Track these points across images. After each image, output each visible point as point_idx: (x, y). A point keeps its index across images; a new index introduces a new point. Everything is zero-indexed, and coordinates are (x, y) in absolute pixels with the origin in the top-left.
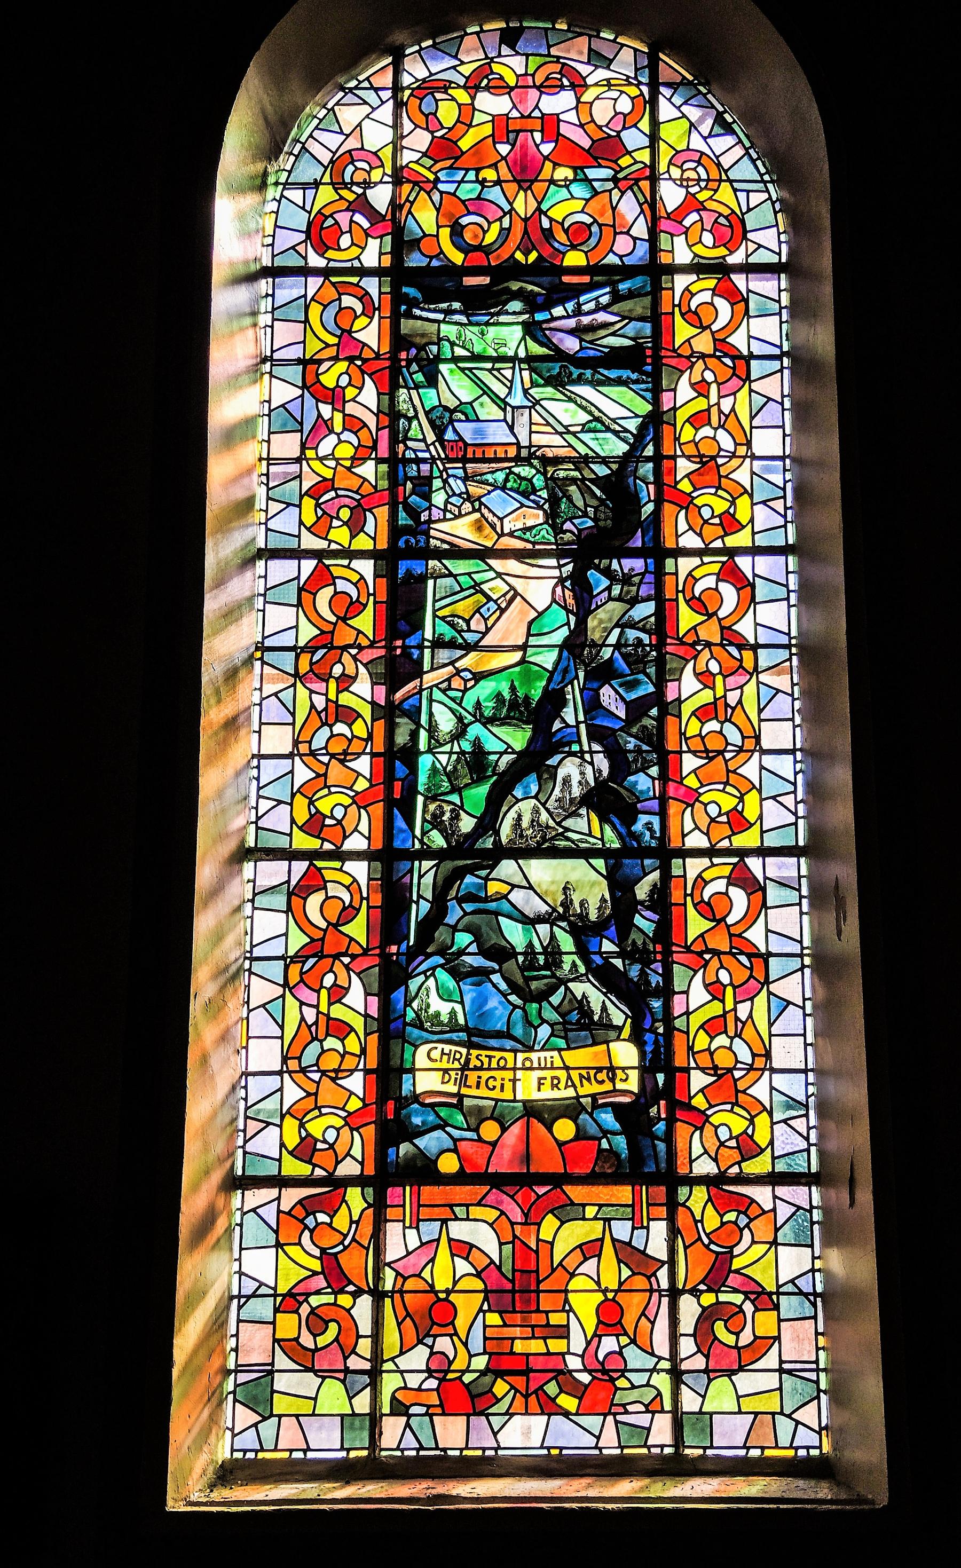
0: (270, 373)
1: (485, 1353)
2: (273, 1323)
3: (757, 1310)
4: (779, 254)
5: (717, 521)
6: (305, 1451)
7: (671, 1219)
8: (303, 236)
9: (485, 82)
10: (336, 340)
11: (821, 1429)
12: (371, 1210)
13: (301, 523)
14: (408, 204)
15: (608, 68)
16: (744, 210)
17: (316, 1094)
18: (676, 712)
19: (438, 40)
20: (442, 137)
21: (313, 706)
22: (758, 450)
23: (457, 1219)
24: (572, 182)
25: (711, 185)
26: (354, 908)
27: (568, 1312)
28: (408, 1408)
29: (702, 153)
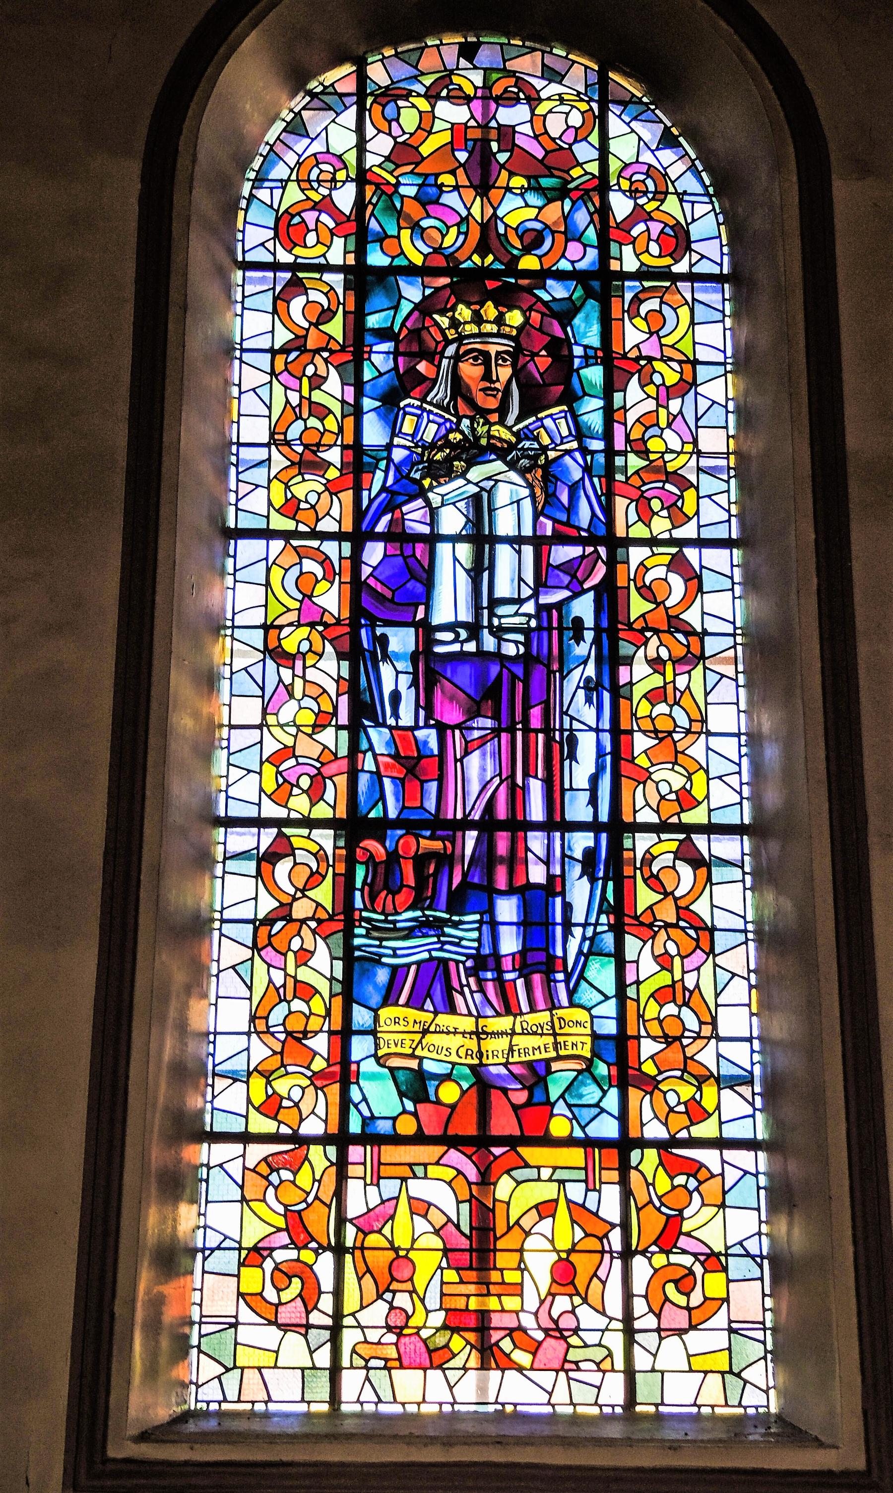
0: (232, 636)
1: (441, 1309)
2: (238, 1276)
3: (706, 1271)
4: (721, 265)
5: (682, 1108)
6: (266, 1403)
7: (624, 1182)
8: (271, 234)
9: (444, 93)
10: (297, 605)
11: (768, 1388)
12: (334, 1168)
13: (270, 504)
14: (370, 207)
15: (560, 83)
16: (689, 220)
17: (281, 1053)
18: (628, 695)
19: (399, 50)
20: (404, 143)
21: (288, 402)
22: (702, 447)
23: (415, 1177)
24: (526, 190)
25: (658, 196)
26: (320, 874)
27: (522, 1271)
28: (367, 1361)
29: (650, 166)
